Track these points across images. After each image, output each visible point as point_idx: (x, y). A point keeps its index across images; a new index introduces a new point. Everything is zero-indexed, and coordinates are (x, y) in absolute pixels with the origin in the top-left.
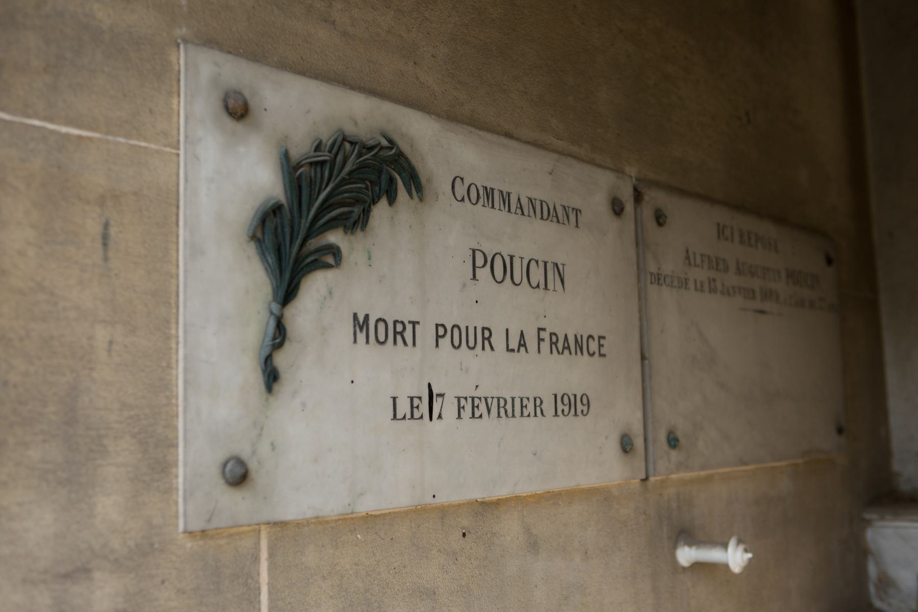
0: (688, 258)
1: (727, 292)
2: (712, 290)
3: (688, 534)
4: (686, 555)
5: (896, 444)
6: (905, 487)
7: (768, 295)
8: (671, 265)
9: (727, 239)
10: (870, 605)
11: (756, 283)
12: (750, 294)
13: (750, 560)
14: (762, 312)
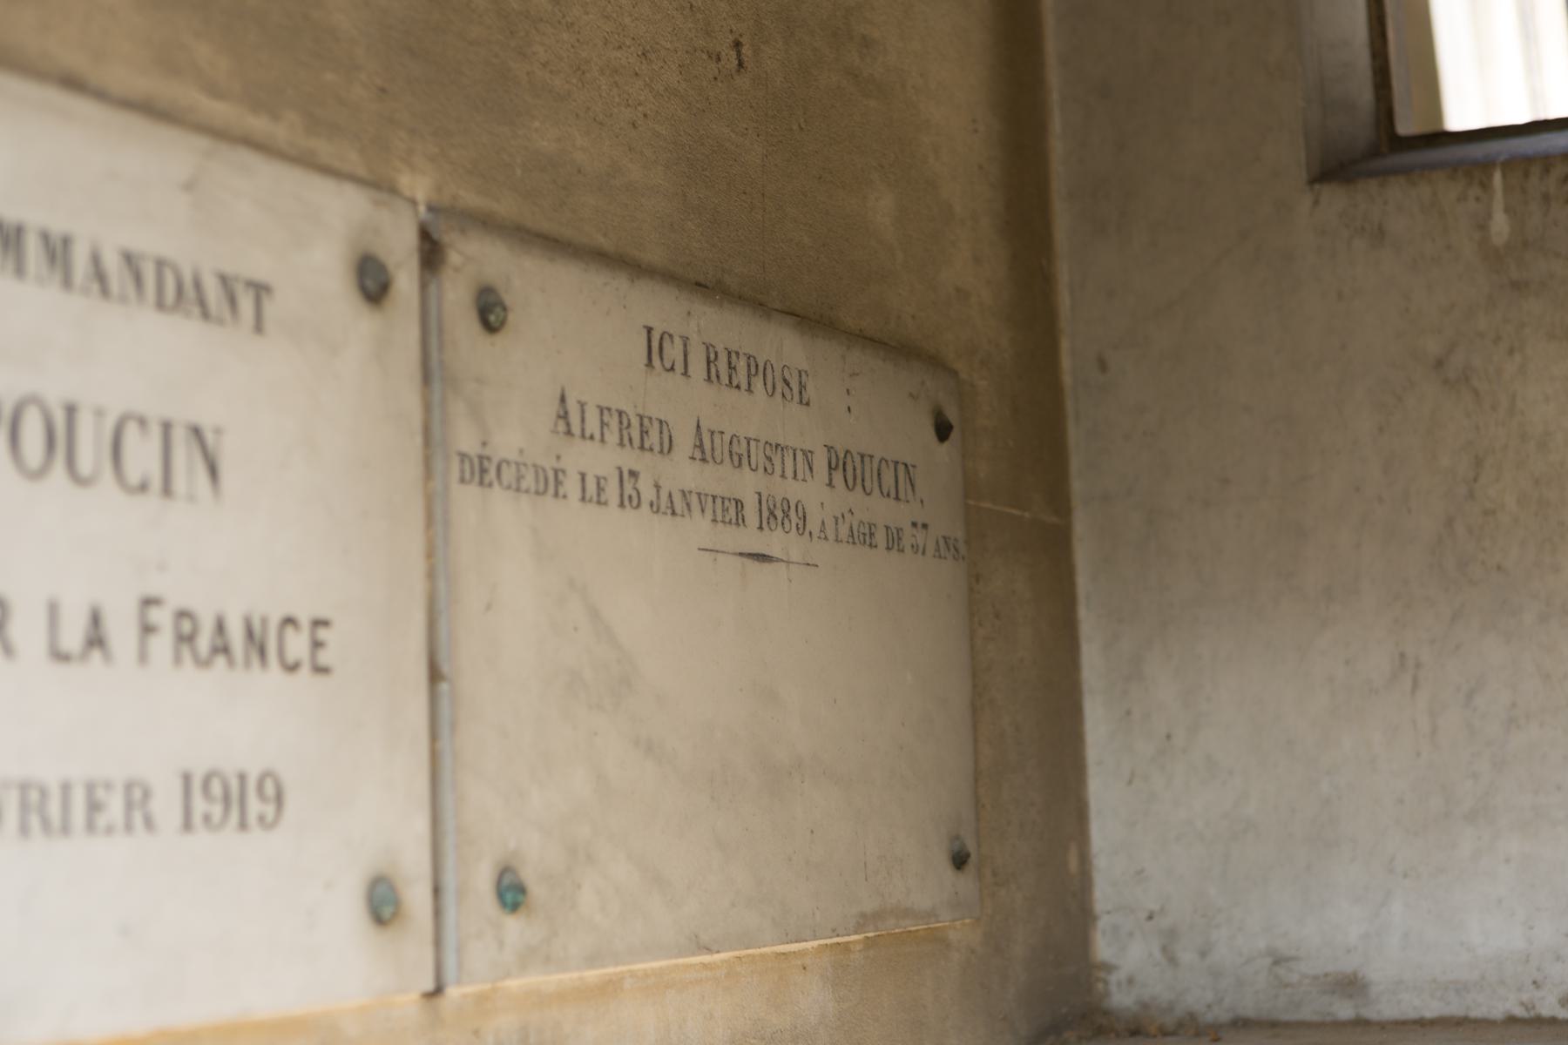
1: (670, 506)
8: (518, 433)
12: (731, 511)
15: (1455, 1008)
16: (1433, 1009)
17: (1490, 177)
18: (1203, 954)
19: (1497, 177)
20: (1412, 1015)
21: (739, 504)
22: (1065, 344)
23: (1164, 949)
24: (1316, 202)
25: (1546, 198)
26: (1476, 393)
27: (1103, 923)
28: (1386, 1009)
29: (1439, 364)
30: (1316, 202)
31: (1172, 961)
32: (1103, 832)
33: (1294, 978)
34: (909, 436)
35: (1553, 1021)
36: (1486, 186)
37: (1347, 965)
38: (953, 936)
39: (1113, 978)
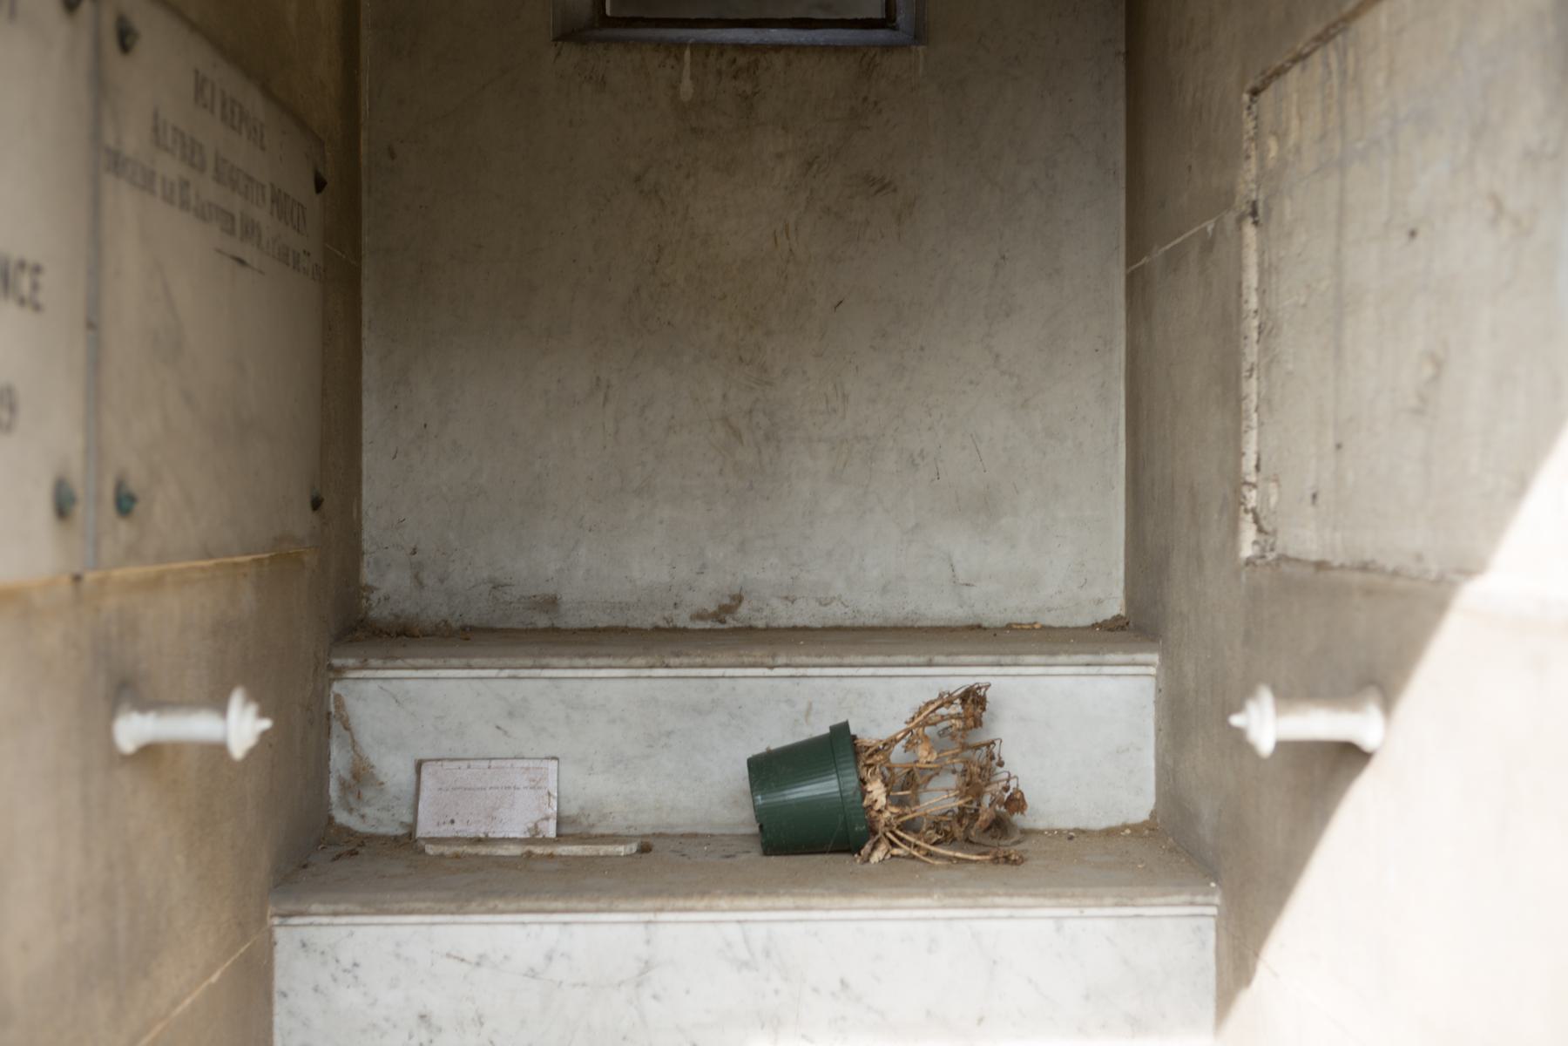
0: (156, 129)
1: (203, 213)
2: (184, 205)
3: (128, 690)
4: (133, 730)
5: (370, 532)
6: (379, 612)
7: (250, 230)
8: (134, 141)
9: (205, 106)
10: (331, 819)
11: (236, 204)
12: (227, 221)
13: (264, 735)
14: (241, 262)
15: (619, 621)
16: (603, 621)
17: (682, 54)
18: (442, 581)
19: (687, 53)
20: (589, 625)
21: (233, 218)
22: (364, 135)
23: (416, 577)
24: (559, 54)
25: (719, 73)
26: (662, 202)
27: (366, 558)
28: (572, 621)
29: (638, 179)
30: (559, 54)
31: (420, 584)
32: (371, 493)
33: (508, 598)
34: (302, 189)
35: (685, 630)
36: (679, 58)
37: (550, 589)
38: (306, 558)
39: (374, 597)
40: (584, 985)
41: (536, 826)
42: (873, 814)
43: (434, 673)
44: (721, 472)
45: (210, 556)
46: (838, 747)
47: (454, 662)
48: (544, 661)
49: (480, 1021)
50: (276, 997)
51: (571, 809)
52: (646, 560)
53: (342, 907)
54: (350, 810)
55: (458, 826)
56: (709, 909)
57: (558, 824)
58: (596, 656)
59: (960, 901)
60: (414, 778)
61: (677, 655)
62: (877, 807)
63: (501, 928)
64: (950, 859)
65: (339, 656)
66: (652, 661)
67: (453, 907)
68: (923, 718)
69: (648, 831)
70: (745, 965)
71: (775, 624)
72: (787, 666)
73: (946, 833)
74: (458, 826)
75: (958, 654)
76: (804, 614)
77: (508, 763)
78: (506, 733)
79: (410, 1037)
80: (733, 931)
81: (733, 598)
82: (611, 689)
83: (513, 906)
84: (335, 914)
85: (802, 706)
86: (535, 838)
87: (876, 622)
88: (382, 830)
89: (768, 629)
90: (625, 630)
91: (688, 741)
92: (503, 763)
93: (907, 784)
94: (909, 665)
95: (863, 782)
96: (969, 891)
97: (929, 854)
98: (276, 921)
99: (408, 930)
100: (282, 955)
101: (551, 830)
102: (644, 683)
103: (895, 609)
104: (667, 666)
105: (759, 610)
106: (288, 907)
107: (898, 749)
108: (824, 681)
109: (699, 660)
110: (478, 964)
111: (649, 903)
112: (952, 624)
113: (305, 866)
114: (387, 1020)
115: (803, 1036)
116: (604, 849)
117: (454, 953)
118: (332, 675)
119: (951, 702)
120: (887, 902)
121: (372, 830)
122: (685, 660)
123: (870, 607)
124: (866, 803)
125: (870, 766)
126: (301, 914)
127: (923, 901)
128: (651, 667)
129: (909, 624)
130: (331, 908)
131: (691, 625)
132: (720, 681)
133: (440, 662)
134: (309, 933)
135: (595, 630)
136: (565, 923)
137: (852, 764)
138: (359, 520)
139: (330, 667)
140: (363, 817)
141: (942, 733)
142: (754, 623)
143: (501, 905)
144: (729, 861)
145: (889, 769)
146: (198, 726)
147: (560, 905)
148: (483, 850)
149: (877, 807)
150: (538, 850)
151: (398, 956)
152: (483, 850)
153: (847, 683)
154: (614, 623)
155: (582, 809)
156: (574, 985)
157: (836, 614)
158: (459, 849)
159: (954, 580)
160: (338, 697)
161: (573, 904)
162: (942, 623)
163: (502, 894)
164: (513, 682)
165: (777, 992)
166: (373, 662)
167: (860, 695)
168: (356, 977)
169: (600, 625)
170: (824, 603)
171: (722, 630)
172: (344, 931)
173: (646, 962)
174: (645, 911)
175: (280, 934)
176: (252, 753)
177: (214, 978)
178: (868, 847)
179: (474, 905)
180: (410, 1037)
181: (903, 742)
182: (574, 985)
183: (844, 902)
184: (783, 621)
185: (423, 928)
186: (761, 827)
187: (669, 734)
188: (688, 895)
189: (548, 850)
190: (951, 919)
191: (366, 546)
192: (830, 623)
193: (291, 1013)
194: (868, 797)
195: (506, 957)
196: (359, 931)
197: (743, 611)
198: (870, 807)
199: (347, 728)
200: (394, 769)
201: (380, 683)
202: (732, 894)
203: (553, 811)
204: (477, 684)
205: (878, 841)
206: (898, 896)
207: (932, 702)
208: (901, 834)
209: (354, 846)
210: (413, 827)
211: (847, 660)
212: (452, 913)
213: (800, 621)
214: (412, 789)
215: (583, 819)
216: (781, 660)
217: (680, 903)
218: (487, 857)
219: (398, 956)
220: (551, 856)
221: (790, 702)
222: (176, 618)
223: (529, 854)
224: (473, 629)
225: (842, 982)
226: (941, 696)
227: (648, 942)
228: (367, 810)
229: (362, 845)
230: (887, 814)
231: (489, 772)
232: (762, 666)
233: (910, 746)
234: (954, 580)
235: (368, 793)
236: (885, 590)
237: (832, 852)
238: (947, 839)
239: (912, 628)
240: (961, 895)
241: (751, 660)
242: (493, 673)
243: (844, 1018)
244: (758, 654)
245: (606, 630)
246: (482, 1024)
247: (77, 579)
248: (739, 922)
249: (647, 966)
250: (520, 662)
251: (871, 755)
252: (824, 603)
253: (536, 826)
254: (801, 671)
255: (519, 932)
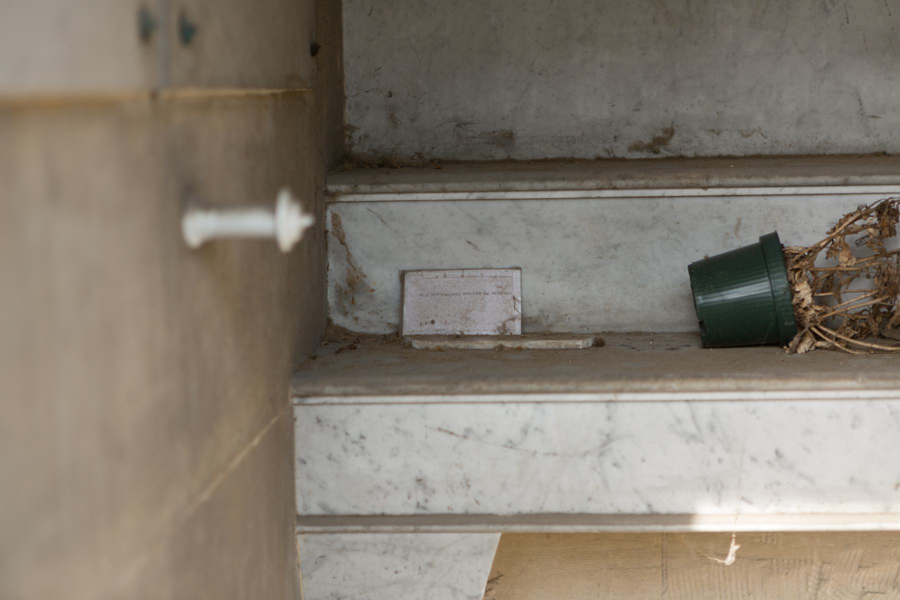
3: (191, 194)
4: (199, 226)
5: (350, 78)
10: (329, 321)
15: (566, 153)
16: (553, 153)
20: (540, 157)
27: (348, 102)
28: (526, 154)
32: (351, 45)
33: (470, 134)
35: (623, 160)
39: (356, 135)
40: (555, 454)
41: (504, 325)
42: (801, 311)
43: (414, 196)
44: (654, 21)
45: (243, 85)
46: (768, 254)
47: (432, 186)
48: (508, 185)
49: (467, 484)
50: (297, 464)
51: (533, 312)
52: (590, 102)
53: (350, 389)
54: (345, 314)
55: (437, 326)
56: (662, 390)
57: (523, 324)
58: (553, 179)
59: (882, 383)
60: (398, 286)
61: (623, 178)
62: (804, 305)
63: (482, 406)
64: (868, 350)
65: (333, 183)
66: (601, 183)
67: (443, 388)
68: (843, 228)
69: (598, 330)
70: (693, 437)
71: (702, 154)
72: (719, 186)
73: (862, 329)
74: (437, 326)
75: (871, 174)
76: (728, 144)
77: (479, 272)
78: (475, 247)
79: (409, 498)
80: (682, 409)
81: (666, 131)
82: (566, 208)
83: (495, 387)
84: (345, 395)
85: (732, 221)
86: (503, 334)
87: (792, 151)
88: (372, 330)
89: (696, 158)
90: (571, 160)
91: (639, 250)
92: (474, 273)
93: (829, 285)
94: (827, 185)
95: (791, 284)
96: (889, 374)
97: (848, 346)
98: (296, 401)
99: (404, 409)
100: (300, 430)
101: (516, 328)
102: (593, 203)
103: (808, 139)
104: (615, 188)
105: (689, 141)
106: (308, 388)
107: (822, 254)
108: (752, 199)
109: (642, 182)
110: (465, 437)
111: (610, 385)
112: (860, 151)
113: (314, 358)
114: (389, 483)
115: (743, 498)
116: (570, 343)
117: (444, 427)
118: (327, 200)
119: (867, 215)
120: (817, 384)
121: (364, 330)
122: (630, 183)
123: (787, 136)
124: (795, 301)
125: (796, 270)
126: (316, 395)
127: (849, 383)
128: (601, 189)
129: (821, 152)
130: (342, 389)
131: (629, 156)
132: (660, 201)
133: (419, 187)
134: (322, 411)
135: (545, 161)
136: (538, 402)
137: (782, 267)
138: (342, 69)
139: (327, 193)
140: (356, 319)
141: (858, 243)
142: (684, 153)
143: (485, 387)
144: (674, 352)
145: (812, 272)
146: (252, 223)
147: (534, 386)
148: (462, 345)
149: (804, 305)
150: (508, 344)
151: (397, 430)
152: (462, 345)
153: (772, 201)
154: (561, 154)
155: (542, 311)
156: (547, 455)
157: (756, 144)
158: (442, 344)
159: (862, 113)
160: (335, 217)
161: (546, 386)
162: (851, 151)
163: (485, 378)
164: (481, 203)
165: (720, 461)
166: (363, 188)
167: (783, 211)
168: (363, 448)
169: (550, 156)
170: (745, 135)
171: (656, 159)
172: (352, 409)
173: (608, 436)
174: (607, 392)
175: (299, 411)
176: (298, 246)
177: (256, 442)
178: (796, 339)
179: (461, 387)
180: (409, 498)
181: (825, 250)
182: (547, 455)
183: (780, 384)
184: (709, 151)
185: (418, 407)
186: (701, 324)
187: (616, 247)
188: (644, 378)
189: (517, 344)
190: (872, 399)
191: (346, 93)
192: (751, 152)
193: (309, 477)
194: (797, 296)
195: (488, 431)
196: (365, 409)
197: (675, 142)
198: (798, 305)
199: (343, 243)
200: (381, 278)
201: (368, 205)
202: (683, 377)
203: (517, 313)
204: (449, 205)
205: (804, 335)
206: (827, 379)
207: (851, 215)
208: (825, 329)
209: (353, 342)
210: (399, 328)
211: (772, 181)
212: (443, 394)
213: (724, 151)
214: (397, 295)
215: (543, 320)
216: (714, 181)
217: (638, 385)
218: (465, 350)
219: (397, 430)
220: (520, 349)
221: (722, 219)
222: (223, 136)
223: (501, 348)
224: (440, 161)
225: (777, 453)
226: (859, 209)
227: (609, 418)
228: (359, 314)
229: (358, 342)
230: (812, 312)
231: (462, 280)
232: (697, 186)
233: (833, 251)
234: (862, 113)
235: (360, 300)
236: (799, 122)
237: (766, 345)
238: (864, 333)
239: (824, 155)
240: (882, 378)
241: (689, 181)
242: (464, 196)
243: (778, 483)
244: (694, 176)
245: (556, 160)
246: (469, 486)
247: (154, 95)
248: (687, 401)
249: (608, 439)
250: (488, 185)
251: (797, 261)
252: (745, 135)
253: (504, 325)
254: (732, 191)
255: (499, 410)
